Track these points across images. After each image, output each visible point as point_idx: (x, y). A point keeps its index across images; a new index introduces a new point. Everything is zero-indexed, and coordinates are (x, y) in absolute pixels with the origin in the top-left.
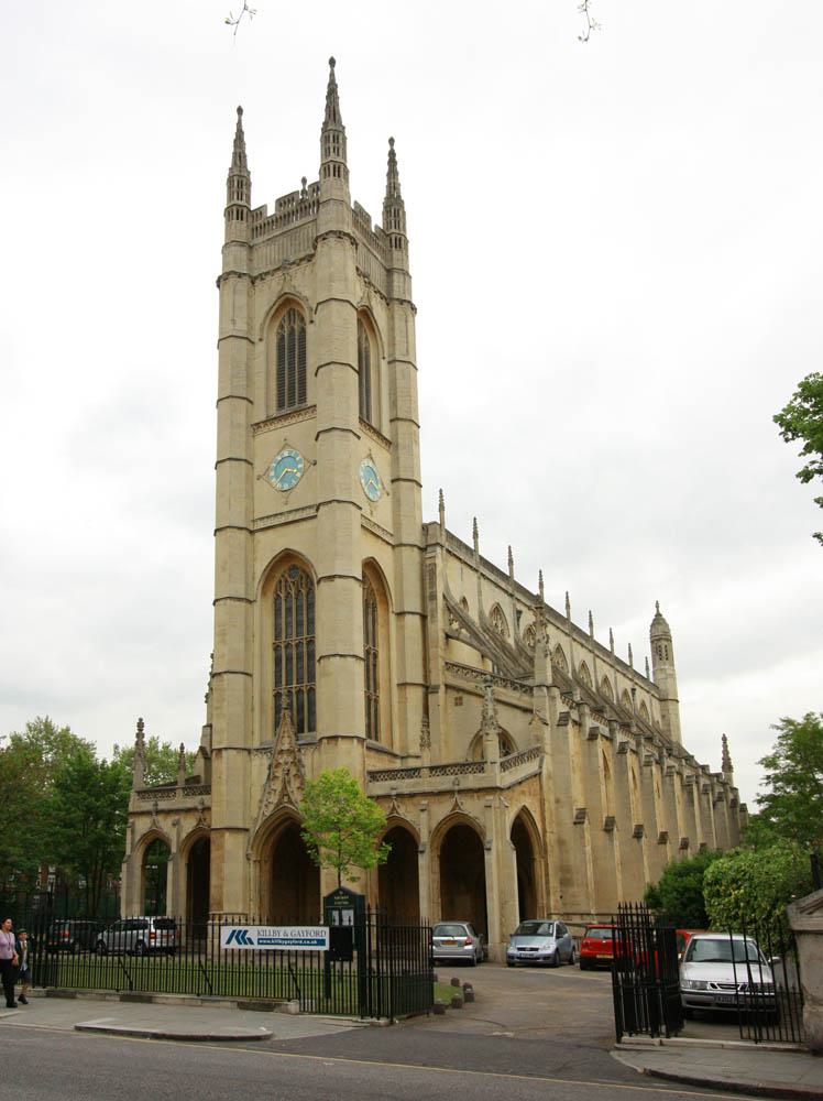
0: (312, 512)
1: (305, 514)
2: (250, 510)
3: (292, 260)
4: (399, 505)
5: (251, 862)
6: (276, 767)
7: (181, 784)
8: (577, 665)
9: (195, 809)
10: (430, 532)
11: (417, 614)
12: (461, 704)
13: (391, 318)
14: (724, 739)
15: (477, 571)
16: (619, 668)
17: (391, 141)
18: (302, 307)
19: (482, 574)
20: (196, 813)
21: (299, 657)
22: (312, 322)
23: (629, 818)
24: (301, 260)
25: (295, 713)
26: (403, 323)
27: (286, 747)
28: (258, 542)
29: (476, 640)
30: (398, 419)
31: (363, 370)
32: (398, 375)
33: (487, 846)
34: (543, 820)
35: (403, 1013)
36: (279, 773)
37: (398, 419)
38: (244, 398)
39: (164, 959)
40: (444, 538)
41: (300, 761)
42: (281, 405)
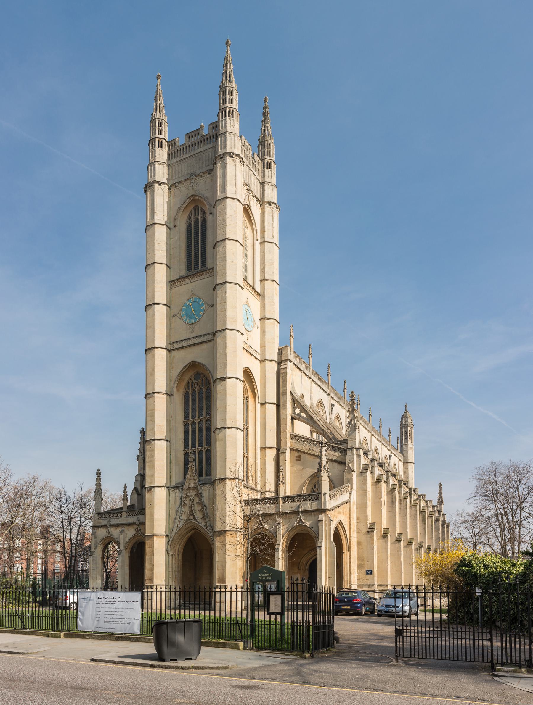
0: (210, 337)
1: (205, 339)
2: (423, 611)
3: (197, 173)
5: (170, 555)
6: (186, 498)
7: (125, 509)
8: (362, 439)
9: (134, 524)
10: (284, 352)
11: (274, 404)
12: (300, 460)
13: (263, 214)
14: (99, 473)
15: (310, 378)
16: (383, 443)
19: (313, 381)
20: (135, 526)
21: (201, 430)
22: (211, 214)
23: (395, 530)
24: (204, 173)
25: (197, 464)
26: (271, 218)
27: (192, 485)
28: (174, 357)
29: (310, 420)
31: (278, 406)
33: (319, 545)
34: (350, 529)
35: (314, 540)
36: (187, 502)
38: (216, 202)
39: (44, 609)
40: (292, 356)
41: (201, 494)
42: (189, 268)
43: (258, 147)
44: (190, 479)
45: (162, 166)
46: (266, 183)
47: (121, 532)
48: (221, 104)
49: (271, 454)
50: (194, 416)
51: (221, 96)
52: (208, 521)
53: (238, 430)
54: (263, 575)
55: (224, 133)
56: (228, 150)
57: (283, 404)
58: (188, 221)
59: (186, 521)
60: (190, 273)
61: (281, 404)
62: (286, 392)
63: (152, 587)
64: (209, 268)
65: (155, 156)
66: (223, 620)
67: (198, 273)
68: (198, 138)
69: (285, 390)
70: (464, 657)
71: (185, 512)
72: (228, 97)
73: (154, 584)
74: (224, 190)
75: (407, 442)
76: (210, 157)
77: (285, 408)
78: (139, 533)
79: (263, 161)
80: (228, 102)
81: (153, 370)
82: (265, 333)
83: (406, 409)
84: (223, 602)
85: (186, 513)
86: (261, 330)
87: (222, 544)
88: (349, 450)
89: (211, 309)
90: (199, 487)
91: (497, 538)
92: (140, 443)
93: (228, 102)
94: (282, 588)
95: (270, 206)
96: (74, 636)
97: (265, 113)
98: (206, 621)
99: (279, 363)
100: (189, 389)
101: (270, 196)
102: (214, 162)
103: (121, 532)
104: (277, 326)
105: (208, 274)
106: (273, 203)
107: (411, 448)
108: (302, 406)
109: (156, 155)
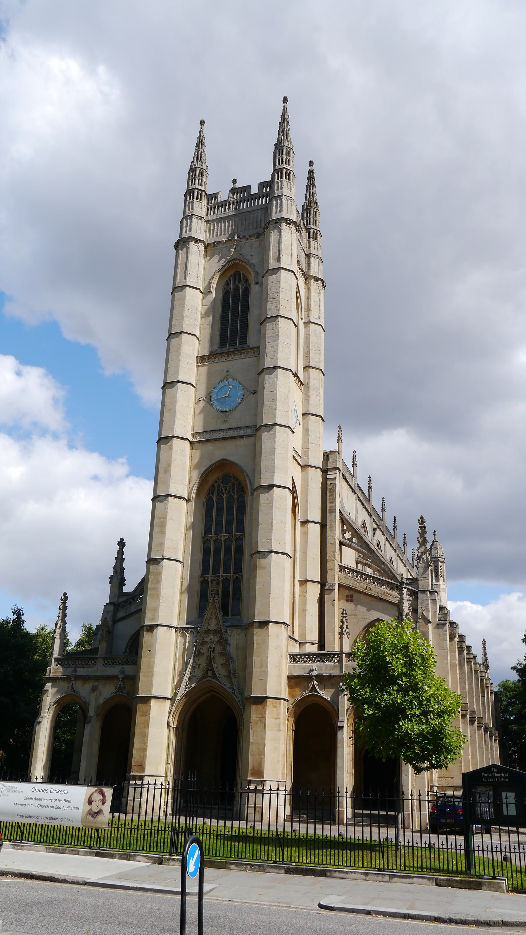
0: (249, 431)
4: (308, 434)
13: (309, 289)
15: (355, 493)
17: (311, 163)
18: (250, 274)
22: (257, 283)
27: (213, 627)
30: (310, 367)
31: (323, 526)
32: (312, 333)
36: (204, 650)
37: (310, 367)
41: (226, 640)
42: (223, 343)
43: (189, 173)
44: (211, 618)
45: (199, 221)
46: (312, 255)
47: (94, 689)
48: (277, 164)
49: (314, 591)
50: (216, 571)
51: (278, 155)
52: (234, 680)
53: (178, 563)
54: (490, 775)
55: (280, 197)
56: (284, 215)
57: (331, 525)
58: (226, 287)
59: (201, 679)
60: (224, 349)
61: (328, 524)
62: (335, 510)
63: (141, 778)
64: (251, 346)
65: (192, 209)
66: (122, 825)
67: (238, 350)
68: (211, 203)
69: (333, 506)
70: (45, 840)
71: (199, 666)
72: (285, 157)
73: (146, 773)
74: (279, 260)
75: (439, 581)
76: (259, 219)
77: (332, 530)
78: (123, 692)
79: (308, 231)
80: (284, 163)
81: (169, 465)
82: (308, 431)
83: (435, 538)
84: (131, 800)
85: (201, 667)
86: (303, 427)
87: (260, 716)
88: (422, 593)
89: (252, 396)
90: (223, 630)
91: (241, 779)
92: (116, 558)
93: (284, 163)
94: (403, 794)
95: (317, 282)
96: (417, 917)
97: (311, 178)
98: (127, 827)
99: (325, 472)
100: (213, 494)
101: (316, 270)
102: (266, 225)
103: (94, 689)
104: (464, 851)
105: (249, 354)
106: (319, 279)
107: (444, 589)
108: (354, 529)
109: (194, 207)
